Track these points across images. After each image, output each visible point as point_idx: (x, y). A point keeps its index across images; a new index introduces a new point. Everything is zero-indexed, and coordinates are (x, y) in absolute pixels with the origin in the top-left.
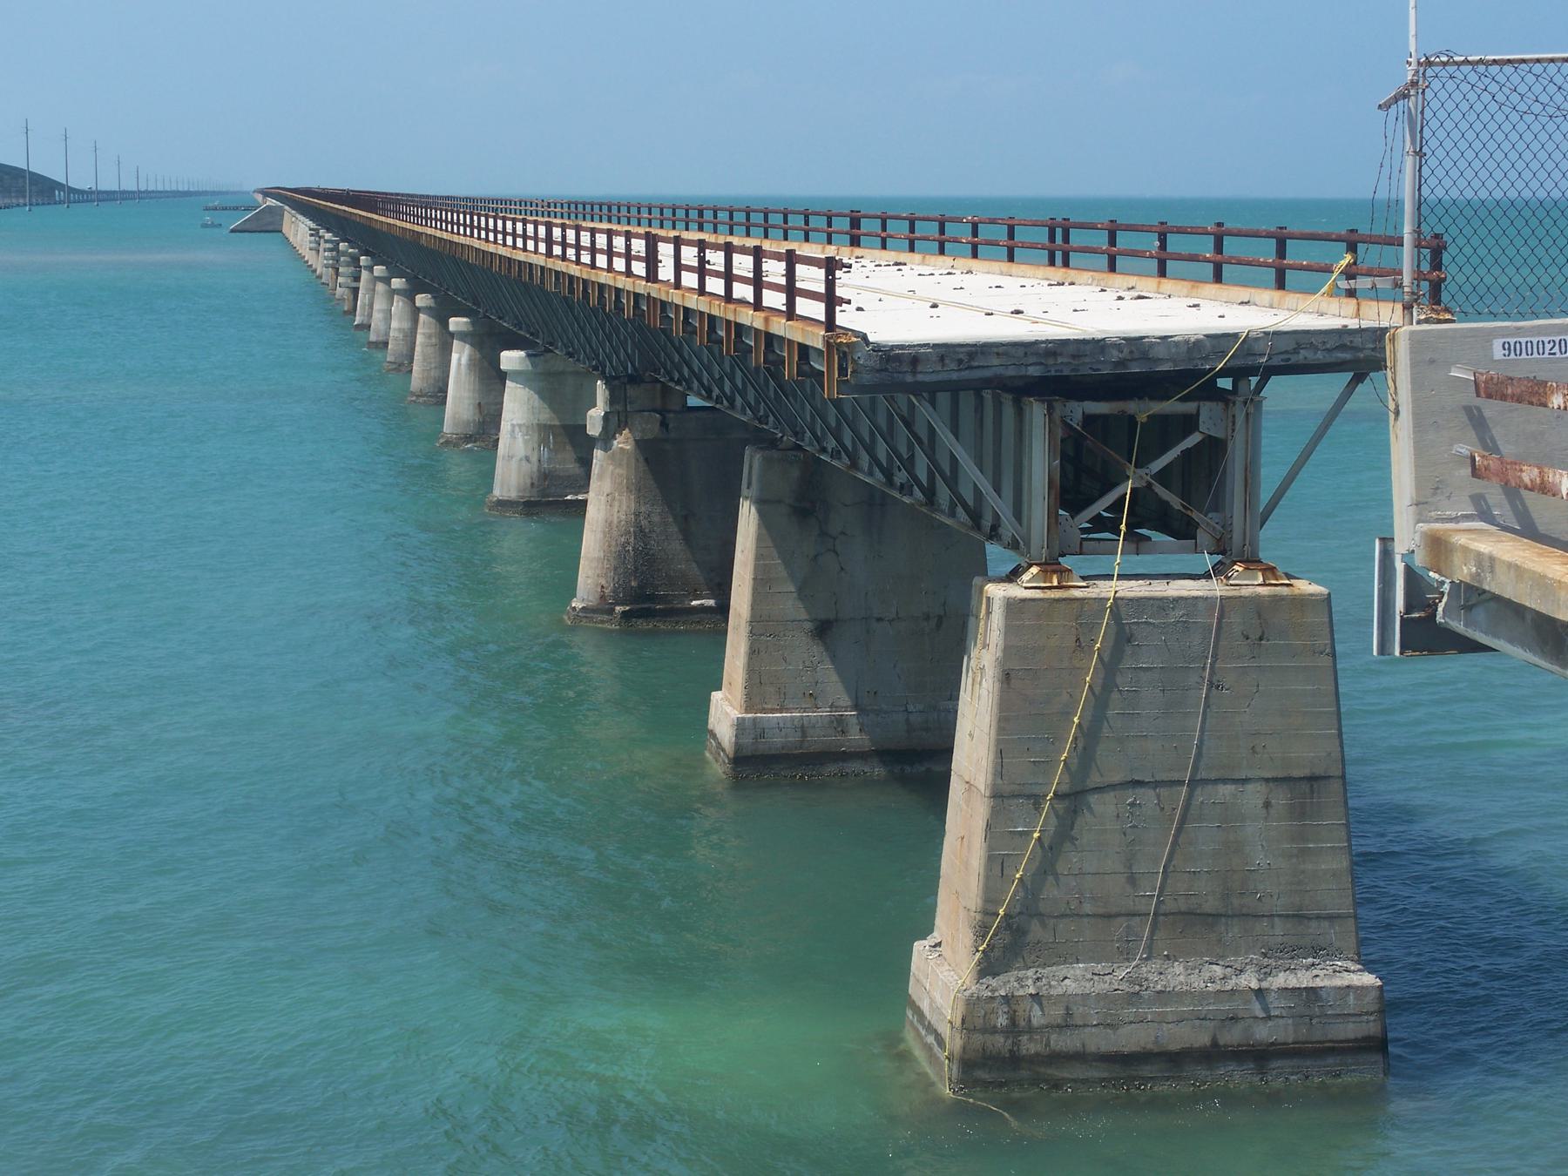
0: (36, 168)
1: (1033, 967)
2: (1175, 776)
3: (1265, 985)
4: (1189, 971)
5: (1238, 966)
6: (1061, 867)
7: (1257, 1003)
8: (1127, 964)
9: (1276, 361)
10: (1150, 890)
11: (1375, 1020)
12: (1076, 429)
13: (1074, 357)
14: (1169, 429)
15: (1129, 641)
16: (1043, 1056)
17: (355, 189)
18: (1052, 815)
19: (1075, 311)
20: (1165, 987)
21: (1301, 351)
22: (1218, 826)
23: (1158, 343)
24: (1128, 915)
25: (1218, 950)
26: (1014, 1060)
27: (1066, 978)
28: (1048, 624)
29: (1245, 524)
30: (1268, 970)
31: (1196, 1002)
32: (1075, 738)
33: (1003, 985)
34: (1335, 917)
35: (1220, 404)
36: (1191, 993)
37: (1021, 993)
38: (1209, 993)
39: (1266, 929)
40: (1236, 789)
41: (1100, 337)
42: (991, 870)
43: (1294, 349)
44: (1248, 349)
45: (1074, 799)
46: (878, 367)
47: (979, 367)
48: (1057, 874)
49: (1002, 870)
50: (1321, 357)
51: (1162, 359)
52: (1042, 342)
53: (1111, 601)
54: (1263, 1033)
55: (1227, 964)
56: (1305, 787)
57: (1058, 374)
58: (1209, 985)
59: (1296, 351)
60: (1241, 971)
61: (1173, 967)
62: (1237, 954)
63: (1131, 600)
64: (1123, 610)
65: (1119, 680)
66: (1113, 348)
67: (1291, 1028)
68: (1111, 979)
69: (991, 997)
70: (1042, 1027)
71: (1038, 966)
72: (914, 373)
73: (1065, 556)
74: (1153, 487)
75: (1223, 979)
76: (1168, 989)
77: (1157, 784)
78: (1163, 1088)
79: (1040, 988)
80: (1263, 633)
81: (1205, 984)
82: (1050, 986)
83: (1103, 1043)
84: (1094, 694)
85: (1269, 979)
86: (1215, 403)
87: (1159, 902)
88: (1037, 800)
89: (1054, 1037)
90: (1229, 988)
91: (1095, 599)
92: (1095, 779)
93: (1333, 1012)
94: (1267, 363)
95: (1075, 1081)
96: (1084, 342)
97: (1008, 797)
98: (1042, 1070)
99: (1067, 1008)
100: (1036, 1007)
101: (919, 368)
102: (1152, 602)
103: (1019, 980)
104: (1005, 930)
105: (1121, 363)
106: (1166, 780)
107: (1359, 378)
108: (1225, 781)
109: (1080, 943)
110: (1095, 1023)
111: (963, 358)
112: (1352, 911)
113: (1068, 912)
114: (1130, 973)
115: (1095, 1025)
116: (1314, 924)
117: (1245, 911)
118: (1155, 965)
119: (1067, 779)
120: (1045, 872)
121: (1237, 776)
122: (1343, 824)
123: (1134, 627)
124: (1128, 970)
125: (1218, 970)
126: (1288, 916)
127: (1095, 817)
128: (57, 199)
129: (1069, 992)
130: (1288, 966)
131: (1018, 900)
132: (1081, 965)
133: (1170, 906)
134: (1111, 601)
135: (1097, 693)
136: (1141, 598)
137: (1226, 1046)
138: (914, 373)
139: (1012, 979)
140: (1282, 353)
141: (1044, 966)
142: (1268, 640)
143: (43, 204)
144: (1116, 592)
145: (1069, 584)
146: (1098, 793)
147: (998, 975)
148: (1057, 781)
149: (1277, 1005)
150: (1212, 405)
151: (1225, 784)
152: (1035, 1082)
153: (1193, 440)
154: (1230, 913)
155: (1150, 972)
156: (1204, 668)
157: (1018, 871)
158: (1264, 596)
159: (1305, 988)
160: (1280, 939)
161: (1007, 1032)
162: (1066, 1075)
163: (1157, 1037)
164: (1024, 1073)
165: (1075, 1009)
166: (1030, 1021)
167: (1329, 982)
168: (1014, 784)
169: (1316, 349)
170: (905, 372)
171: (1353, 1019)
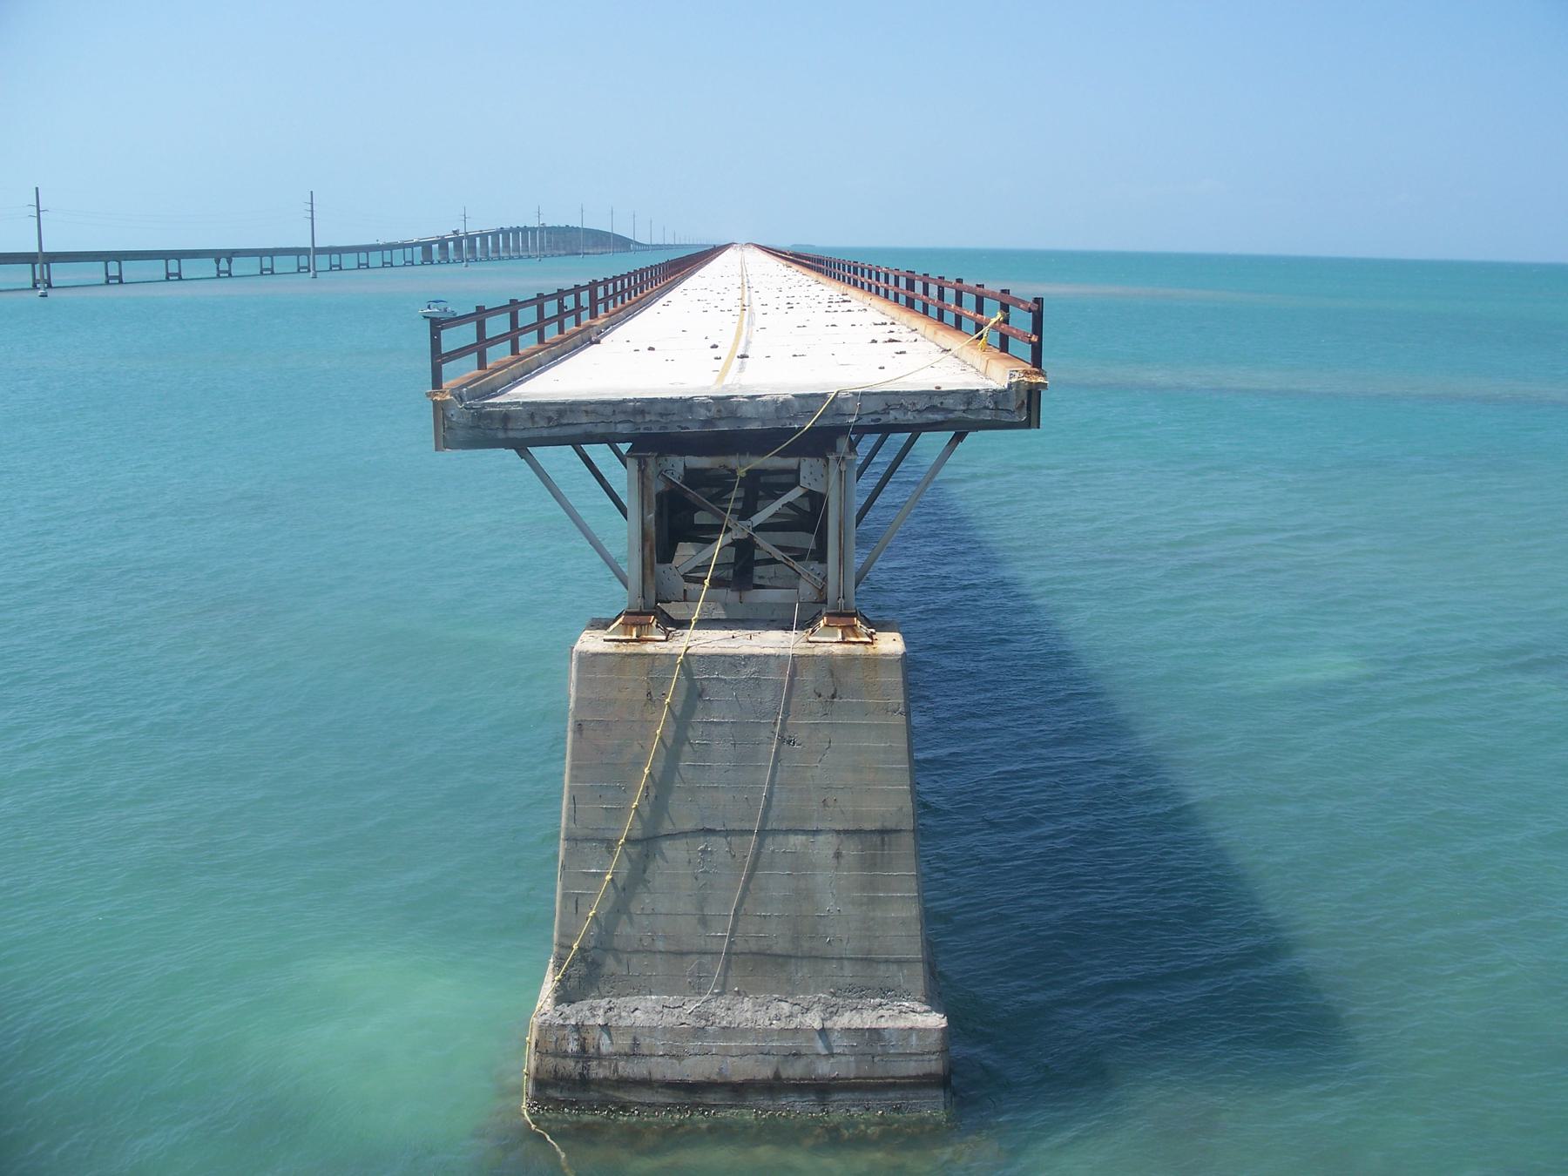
1: (608, 997)
2: (747, 826)
3: (828, 1024)
4: (757, 1008)
5: (805, 1004)
6: (635, 908)
7: (820, 1041)
8: (699, 998)
9: (866, 421)
10: (721, 931)
11: (936, 1060)
13: (661, 415)
14: (760, 488)
15: (700, 696)
16: (610, 1080)
18: (625, 858)
19: (795, 356)
20: (730, 1023)
21: (891, 412)
22: (788, 874)
24: (698, 953)
25: (788, 988)
26: (584, 1082)
27: (637, 1009)
28: (619, 678)
29: (840, 579)
30: (834, 1009)
31: (760, 1038)
32: (647, 788)
33: (575, 1013)
34: (904, 962)
36: (755, 1030)
37: (591, 1022)
38: (773, 1030)
39: (835, 970)
40: (807, 840)
42: (566, 908)
43: (884, 410)
44: (838, 409)
45: (647, 844)
46: (470, 424)
47: (569, 424)
48: (631, 913)
49: (577, 908)
50: (912, 418)
51: (750, 418)
52: (630, 401)
53: (681, 657)
54: (824, 1069)
55: (795, 1002)
56: (876, 839)
57: (646, 431)
58: (774, 1022)
59: (886, 411)
60: (808, 1009)
61: (742, 1003)
62: (806, 992)
63: (702, 656)
64: (694, 666)
65: (690, 733)
66: (700, 407)
67: (853, 1065)
68: (680, 1012)
69: (563, 1025)
70: (611, 1055)
71: (612, 996)
72: (506, 430)
73: (669, 602)
75: (789, 1016)
76: (733, 1026)
77: (728, 833)
78: (730, 1114)
79: (610, 1019)
80: (836, 690)
81: (769, 1022)
82: (620, 1017)
83: (669, 1071)
84: (665, 746)
85: (835, 1018)
86: (815, 460)
87: (731, 943)
88: (610, 844)
89: (621, 1064)
90: (793, 1026)
91: (666, 654)
92: (667, 827)
93: (897, 1051)
94: (856, 424)
95: (642, 1104)
96: (671, 400)
97: (582, 841)
98: (611, 1093)
99: (635, 1039)
100: (605, 1036)
101: (510, 426)
102: (723, 658)
103: (592, 1009)
104: (581, 962)
105: (709, 422)
106: (737, 829)
107: (959, 437)
108: (796, 832)
109: (653, 978)
110: (661, 1053)
111: (553, 416)
112: (920, 956)
113: (641, 948)
114: (699, 1007)
115: (661, 1056)
116: (882, 967)
117: (813, 953)
118: (724, 1001)
119: (639, 825)
120: (618, 911)
121: (808, 827)
122: (913, 875)
123: (705, 683)
124: (697, 1005)
125: (786, 1007)
126: (857, 959)
127: (667, 862)
129: (637, 1024)
130: (855, 1005)
131: (592, 936)
132: (653, 997)
133: (740, 946)
134: (681, 657)
135: (668, 745)
136: (713, 655)
137: (788, 1079)
138: (506, 430)
139: (586, 1008)
140: (872, 413)
141: (619, 996)
142: (841, 698)
144: (688, 648)
145: (649, 637)
146: (670, 840)
147: (574, 1003)
148: (629, 826)
149: (840, 1044)
151: (797, 834)
152: (603, 1105)
153: (793, 495)
154: (800, 954)
155: (718, 1007)
156: (775, 724)
157: (591, 909)
158: (837, 655)
159: (867, 1029)
160: (849, 980)
161: (578, 1057)
162: (633, 1098)
163: (720, 1069)
164: (594, 1095)
165: (642, 1039)
166: (599, 1048)
167: (893, 1024)
168: (587, 828)
169: (906, 410)
171: (915, 1058)
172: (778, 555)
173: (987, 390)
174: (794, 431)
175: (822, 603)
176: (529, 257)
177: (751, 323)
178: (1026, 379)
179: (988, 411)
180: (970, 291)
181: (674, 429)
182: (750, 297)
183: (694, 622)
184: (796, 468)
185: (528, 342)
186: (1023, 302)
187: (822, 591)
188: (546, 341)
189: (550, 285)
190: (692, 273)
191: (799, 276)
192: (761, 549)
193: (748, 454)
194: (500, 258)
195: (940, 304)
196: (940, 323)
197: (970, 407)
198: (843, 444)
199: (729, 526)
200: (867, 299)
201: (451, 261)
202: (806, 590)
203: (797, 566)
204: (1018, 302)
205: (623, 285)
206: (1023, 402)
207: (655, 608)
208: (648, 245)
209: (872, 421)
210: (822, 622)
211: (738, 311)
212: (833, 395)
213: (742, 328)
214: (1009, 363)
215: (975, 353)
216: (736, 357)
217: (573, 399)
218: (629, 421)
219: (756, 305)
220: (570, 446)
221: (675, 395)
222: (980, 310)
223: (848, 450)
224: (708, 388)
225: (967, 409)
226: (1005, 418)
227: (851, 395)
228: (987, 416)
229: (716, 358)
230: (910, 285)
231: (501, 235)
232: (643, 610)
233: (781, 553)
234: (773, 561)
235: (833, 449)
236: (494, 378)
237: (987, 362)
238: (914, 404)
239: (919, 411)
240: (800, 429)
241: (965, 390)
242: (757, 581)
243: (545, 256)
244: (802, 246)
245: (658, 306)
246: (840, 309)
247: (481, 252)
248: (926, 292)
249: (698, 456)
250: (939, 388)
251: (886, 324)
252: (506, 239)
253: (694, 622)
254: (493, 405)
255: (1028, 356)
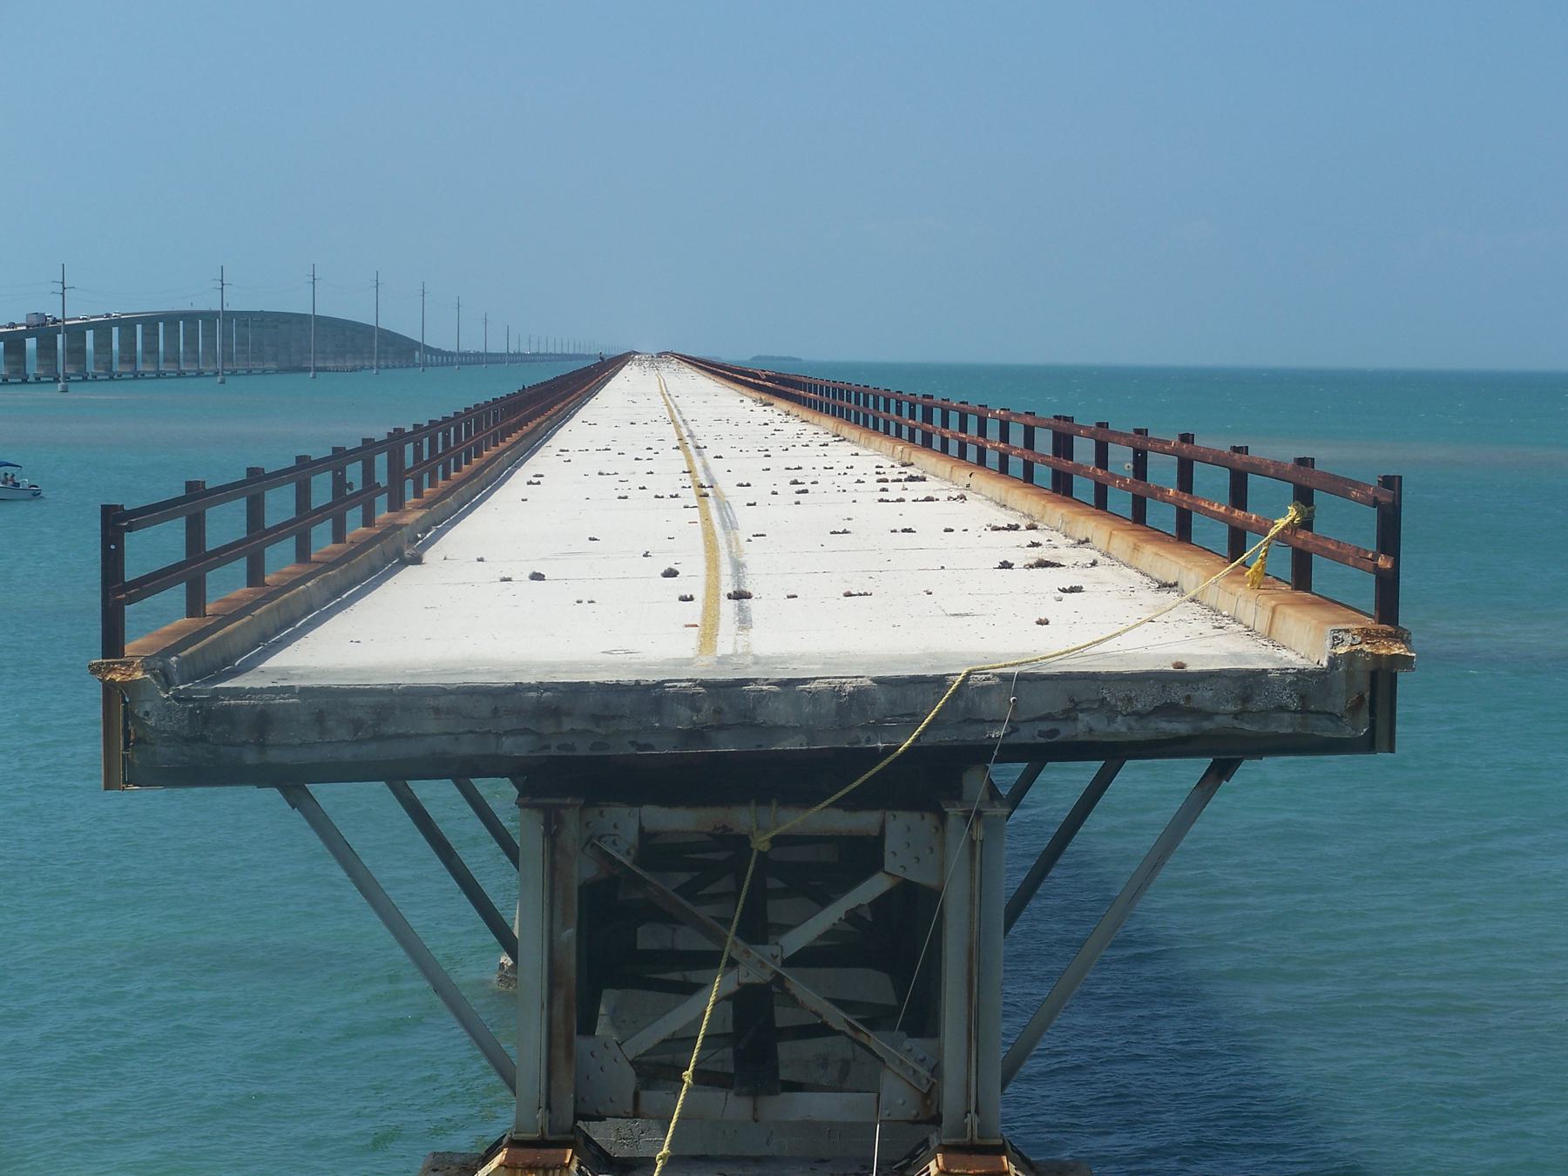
0: (389, 323)
12: (620, 863)
13: (596, 718)
17: (687, 354)
21: (1080, 715)
23: (776, 694)
29: (969, 1069)
35: (928, 816)
41: (653, 678)
43: (1065, 711)
50: (1124, 729)
52: (530, 687)
57: (563, 753)
59: (1069, 715)
72: (262, 746)
73: (602, 1118)
74: (787, 985)
86: (917, 815)
96: (617, 688)
105: (696, 734)
107: (1222, 770)
128: (417, 361)
143: (394, 367)
150: (912, 818)
170: (245, 743)
172: (837, 1018)
173: (1284, 672)
174: (877, 755)
175: (927, 1122)
176: (200, 374)
177: (730, 525)
178: (1367, 648)
179: (1286, 716)
180: (1217, 460)
181: (621, 748)
182: (706, 468)
183: (660, 1164)
184: (875, 832)
185: (280, 560)
186: (1356, 484)
187: (929, 1097)
188: (313, 557)
189: (351, 434)
190: (566, 416)
191: (794, 426)
192: (794, 1001)
193: (774, 802)
194: (137, 376)
195: (1140, 488)
196: (1138, 526)
197: (1250, 707)
198: (974, 784)
199: (734, 955)
200: (962, 475)
201: (31, 379)
202: (897, 1096)
203: (877, 1041)
204: (1340, 486)
205: (446, 439)
206: (1361, 698)
207: (572, 1132)
208: (450, 354)
209: (1041, 734)
210: (932, 1164)
211: (690, 496)
212: (960, 678)
213: (713, 534)
214: (1327, 615)
215: (1240, 591)
216: (724, 598)
217: (408, 681)
218: (526, 731)
219: (727, 485)
220: (272, 795)
221: (626, 677)
222: (1239, 497)
223: (987, 797)
224: (688, 662)
225: (1241, 712)
226: (1326, 730)
227: (998, 680)
228: (1283, 726)
229: (684, 599)
230: (1063, 445)
231: (161, 324)
232: (548, 1137)
233: (842, 1014)
234: (823, 1030)
235: (956, 795)
236: (226, 635)
237: (1274, 611)
238: (1130, 699)
239: (1139, 715)
240: (889, 751)
241: (1237, 671)
242: (784, 1074)
243: (234, 373)
244: (772, 358)
245: (516, 485)
246: (908, 496)
247: (96, 362)
248: (1102, 459)
249: (669, 807)
250: (1181, 666)
251: (1016, 528)
252: (151, 335)
253: (660, 1164)
254: (237, 693)
255: (1369, 603)
